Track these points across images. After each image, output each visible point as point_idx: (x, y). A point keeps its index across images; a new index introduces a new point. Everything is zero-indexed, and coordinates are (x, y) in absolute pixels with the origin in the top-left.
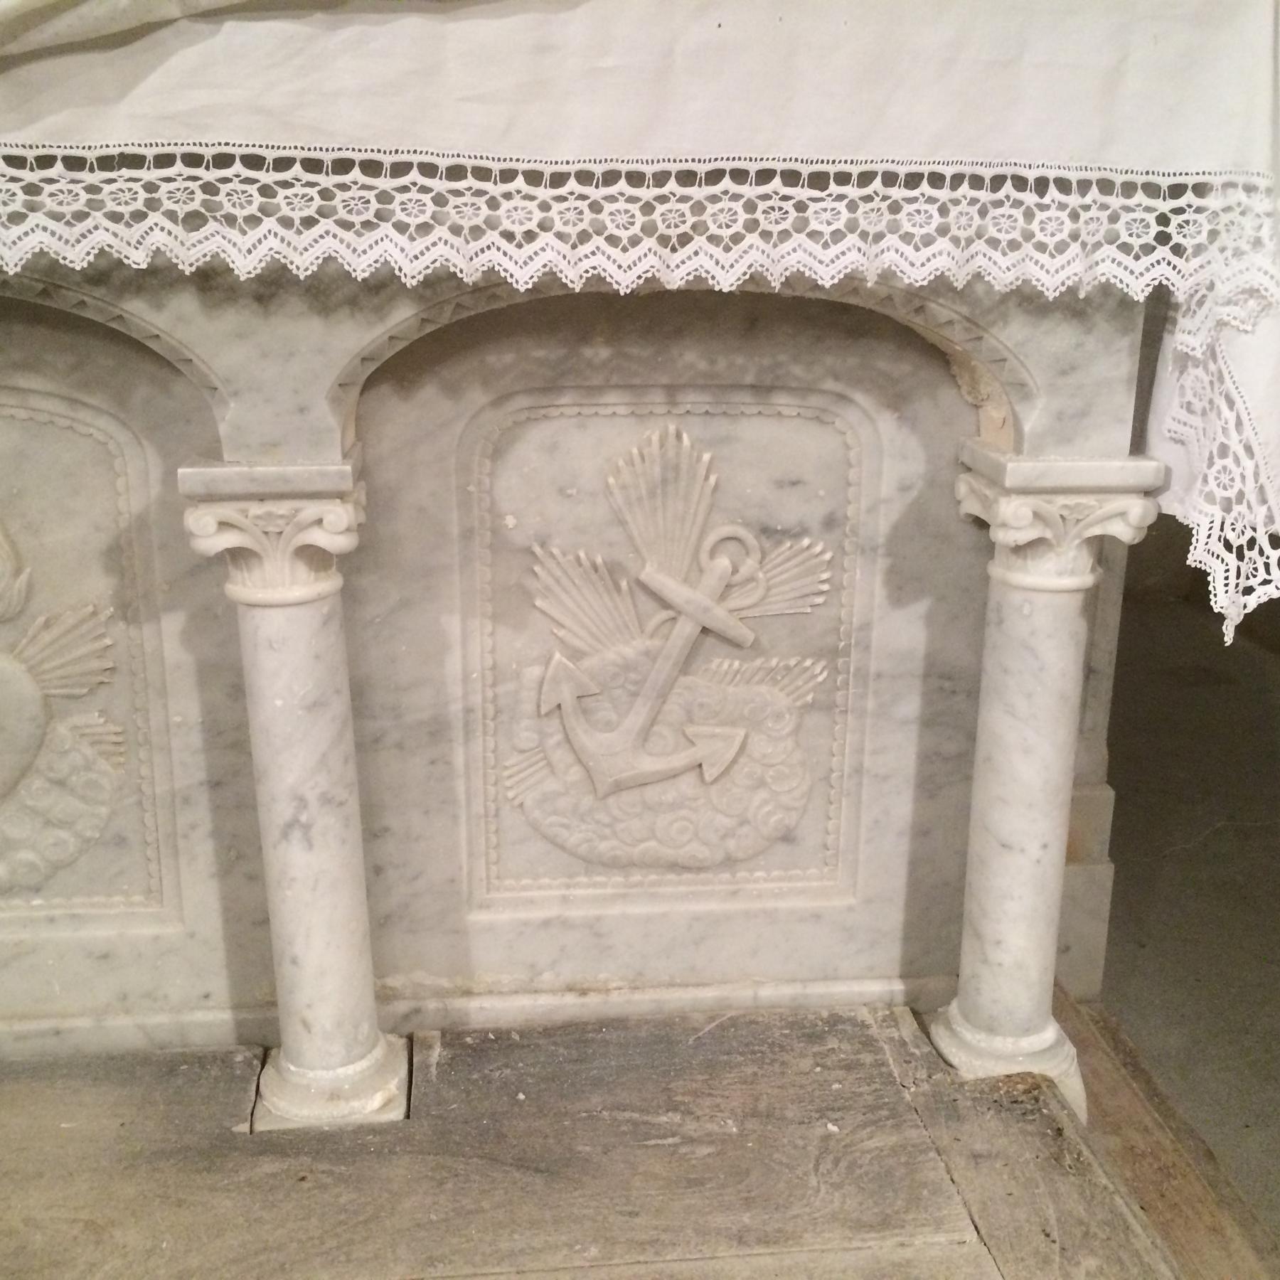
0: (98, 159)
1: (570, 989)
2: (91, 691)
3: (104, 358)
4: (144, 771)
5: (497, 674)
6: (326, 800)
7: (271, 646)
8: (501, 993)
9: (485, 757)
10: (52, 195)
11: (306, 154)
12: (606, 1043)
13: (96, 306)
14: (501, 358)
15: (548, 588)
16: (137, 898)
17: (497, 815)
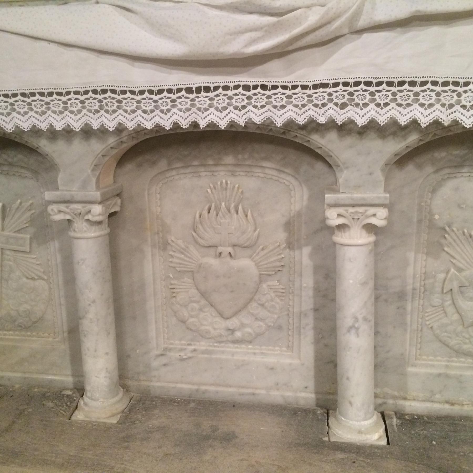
0: (84, 92)
1: (447, 402)
2: (276, 273)
3: (292, 154)
4: (291, 303)
5: (426, 276)
6: (365, 319)
7: (351, 261)
8: (418, 400)
9: (418, 308)
10: (295, 99)
11: (388, 80)
12: (465, 426)
13: (300, 138)
14: (440, 154)
15: (450, 243)
16: (285, 349)
17: (421, 331)
